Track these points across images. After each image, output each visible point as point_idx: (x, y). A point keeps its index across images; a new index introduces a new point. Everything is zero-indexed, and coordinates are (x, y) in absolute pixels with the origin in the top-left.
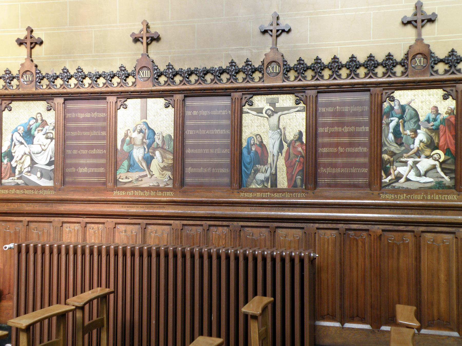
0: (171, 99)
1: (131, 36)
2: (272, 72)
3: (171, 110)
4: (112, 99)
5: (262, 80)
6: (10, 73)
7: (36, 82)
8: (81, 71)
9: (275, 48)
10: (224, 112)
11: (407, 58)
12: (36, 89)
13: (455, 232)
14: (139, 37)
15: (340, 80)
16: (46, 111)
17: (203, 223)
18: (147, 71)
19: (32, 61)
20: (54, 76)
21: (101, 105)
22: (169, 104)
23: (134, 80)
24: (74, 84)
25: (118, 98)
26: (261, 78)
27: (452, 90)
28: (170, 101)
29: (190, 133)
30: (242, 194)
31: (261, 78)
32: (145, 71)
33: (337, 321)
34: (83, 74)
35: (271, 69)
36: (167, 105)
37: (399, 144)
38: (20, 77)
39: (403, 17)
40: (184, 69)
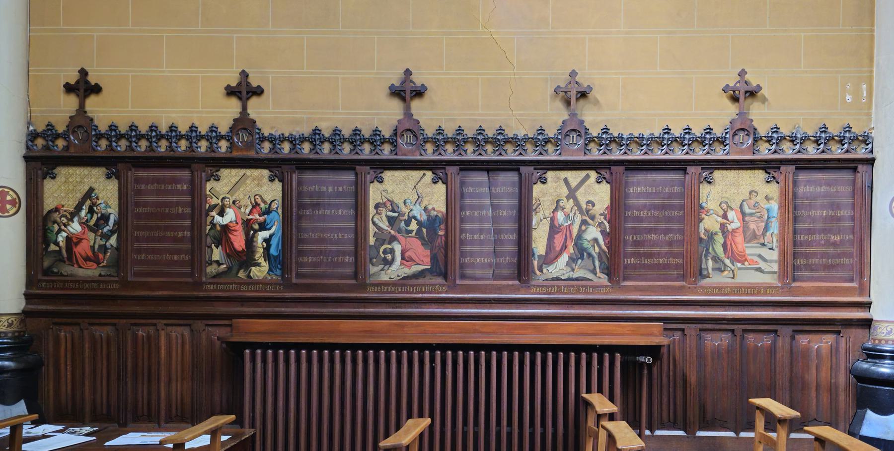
9: (408, 114)
10: (510, 190)
11: (396, 134)
13: (156, 324)
14: (400, 91)
15: (547, 156)
16: (269, 183)
31: (353, 150)
34: (54, 133)
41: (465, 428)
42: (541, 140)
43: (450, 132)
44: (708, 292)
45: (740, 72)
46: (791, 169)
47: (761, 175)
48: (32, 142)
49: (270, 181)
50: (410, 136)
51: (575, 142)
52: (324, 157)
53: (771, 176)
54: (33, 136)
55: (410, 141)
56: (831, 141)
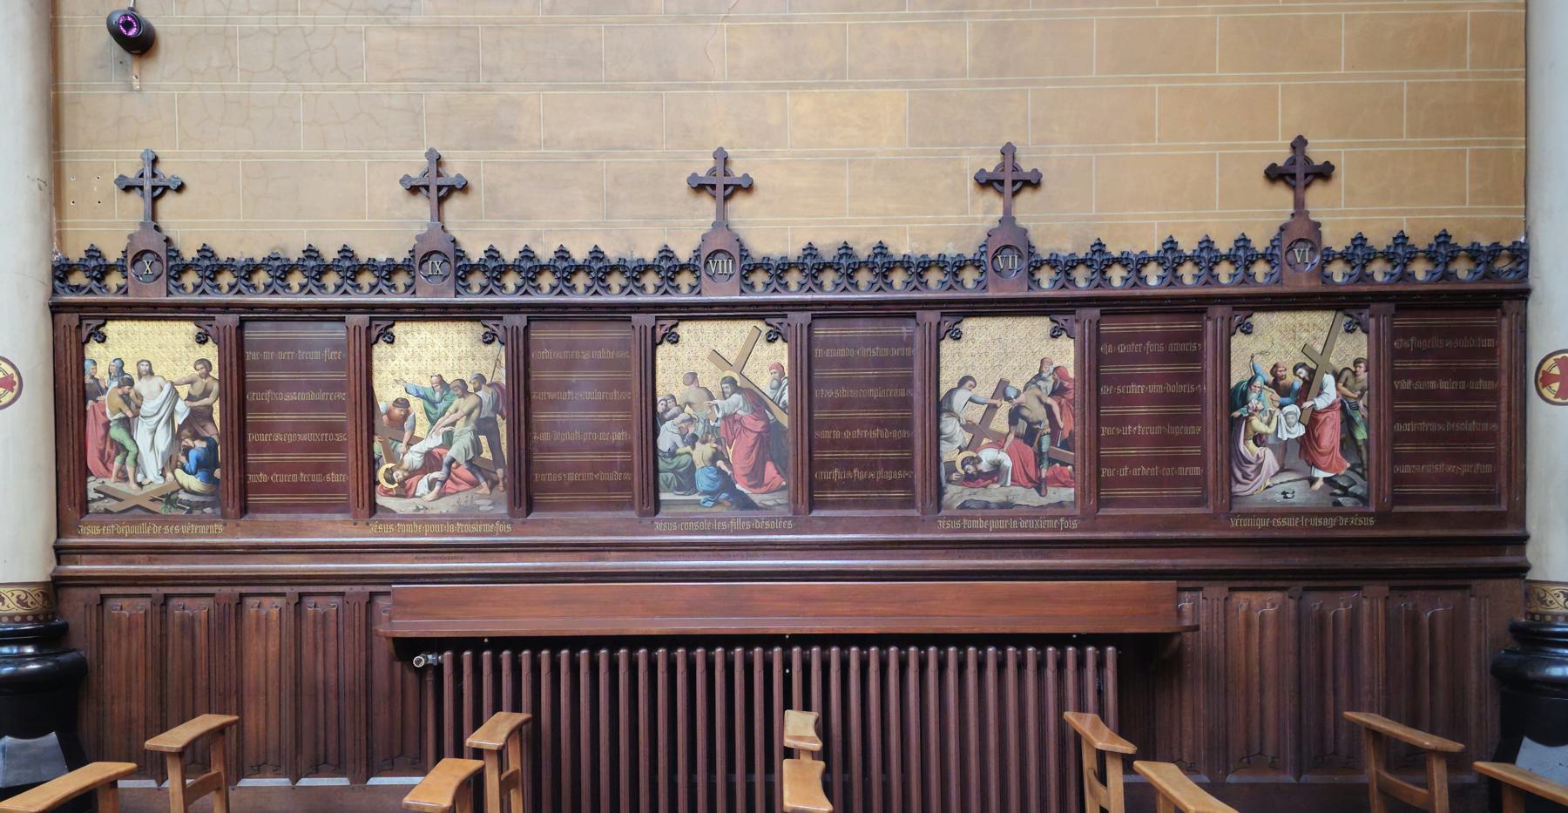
0: (211, 326)
1: (401, 181)
2: (150, 273)
3: (496, 349)
4: (932, 317)
5: (411, 290)
6: (212, 256)
7: (169, 277)
8: (316, 255)
9: (722, 224)
11: (697, 257)
12: (169, 293)
16: (197, 346)
17: (286, 589)
18: (725, 261)
19: (157, 228)
20: (249, 265)
21: (904, 329)
22: (778, 333)
23: (408, 281)
24: (193, 284)
25: (943, 314)
26: (410, 286)
27: (497, 325)
28: (208, 328)
29: (255, 397)
30: (374, 527)
31: (660, 287)
32: (720, 261)
33: (151, 778)
35: (148, 266)
36: (202, 339)
37: (964, 422)
38: (129, 266)
39: (977, 171)
40: (378, 259)
41: (829, 775)
42: (669, 267)
43: (863, 251)
44: (945, 526)
45: (1004, 148)
46: (803, 318)
47: (1042, 325)
48: (62, 280)
49: (199, 343)
50: (723, 262)
51: (725, 272)
52: (1077, 293)
53: (1355, 321)
54: (61, 272)
55: (723, 271)
56: (1338, 261)
